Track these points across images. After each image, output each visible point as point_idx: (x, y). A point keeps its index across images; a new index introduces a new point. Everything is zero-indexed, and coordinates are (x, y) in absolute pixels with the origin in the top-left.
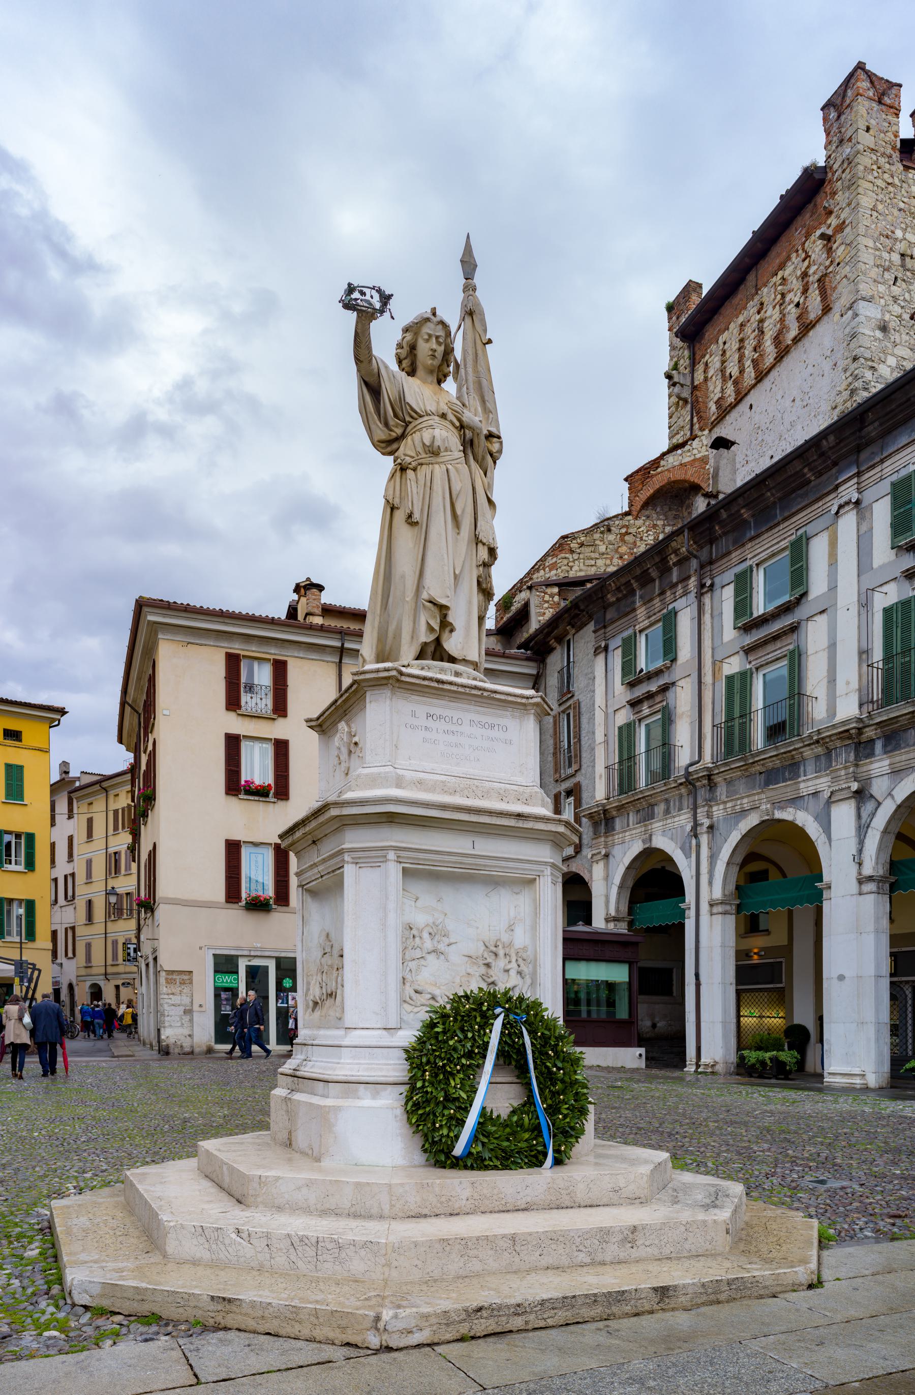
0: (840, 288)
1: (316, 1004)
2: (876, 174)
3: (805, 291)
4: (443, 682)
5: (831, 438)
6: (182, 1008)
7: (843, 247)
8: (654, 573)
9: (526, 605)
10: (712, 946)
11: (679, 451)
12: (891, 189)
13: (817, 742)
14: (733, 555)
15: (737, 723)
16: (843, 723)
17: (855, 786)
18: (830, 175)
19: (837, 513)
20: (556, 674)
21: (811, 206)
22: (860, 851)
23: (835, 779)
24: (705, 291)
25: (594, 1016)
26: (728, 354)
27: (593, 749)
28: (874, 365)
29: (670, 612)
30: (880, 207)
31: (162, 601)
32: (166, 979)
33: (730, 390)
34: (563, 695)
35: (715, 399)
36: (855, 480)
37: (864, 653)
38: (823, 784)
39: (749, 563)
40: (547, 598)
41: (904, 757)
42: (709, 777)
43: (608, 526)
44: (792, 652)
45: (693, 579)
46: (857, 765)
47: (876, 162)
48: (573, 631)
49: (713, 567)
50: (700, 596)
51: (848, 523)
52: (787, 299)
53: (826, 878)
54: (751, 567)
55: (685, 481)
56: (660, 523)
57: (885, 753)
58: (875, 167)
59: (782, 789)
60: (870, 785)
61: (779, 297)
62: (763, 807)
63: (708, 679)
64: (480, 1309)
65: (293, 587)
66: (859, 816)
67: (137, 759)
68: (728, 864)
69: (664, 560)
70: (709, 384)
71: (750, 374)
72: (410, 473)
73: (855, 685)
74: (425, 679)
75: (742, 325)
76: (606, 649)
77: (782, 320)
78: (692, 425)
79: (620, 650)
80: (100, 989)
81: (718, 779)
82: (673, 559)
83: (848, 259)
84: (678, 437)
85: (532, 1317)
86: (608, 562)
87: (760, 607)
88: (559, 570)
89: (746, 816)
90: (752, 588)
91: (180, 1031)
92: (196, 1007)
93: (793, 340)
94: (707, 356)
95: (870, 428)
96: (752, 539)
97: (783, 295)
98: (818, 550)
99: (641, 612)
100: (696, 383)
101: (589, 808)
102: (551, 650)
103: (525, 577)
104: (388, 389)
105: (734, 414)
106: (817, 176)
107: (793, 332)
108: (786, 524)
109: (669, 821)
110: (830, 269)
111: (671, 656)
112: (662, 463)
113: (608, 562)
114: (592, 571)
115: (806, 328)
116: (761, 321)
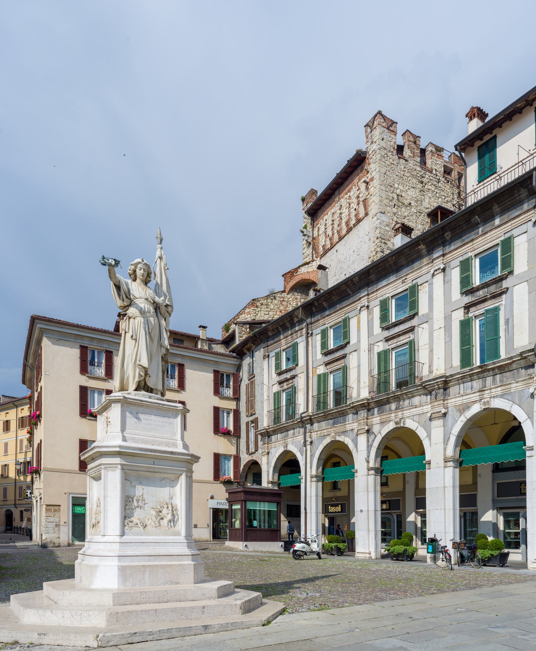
0: (372, 205)
1: (94, 526)
2: (386, 159)
3: (358, 204)
4: (143, 401)
5: (357, 278)
6: (54, 524)
7: (373, 188)
8: (288, 325)
9: (234, 331)
10: (311, 495)
11: (307, 266)
12: (392, 166)
13: (352, 407)
14: (320, 321)
15: (322, 395)
16: (362, 400)
17: (366, 428)
18: (368, 155)
19: (360, 310)
20: (247, 365)
21: (360, 167)
22: (368, 456)
23: (359, 424)
24: (319, 194)
25: (262, 527)
26: (328, 225)
27: (263, 402)
28: (386, 242)
29: (295, 343)
30: (388, 173)
31: (45, 317)
32: (46, 509)
33: (328, 242)
34: (250, 376)
35: (322, 245)
36: (367, 297)
37: (370, 371)
38: (355, 426)
39: (326, 326)
40: (244, 329)
41: (385, 417)
42: (311, 419)
43: (274, 297)
44: (344, 367)
45: (304, 330)
46: (367, 419)
47: (386, 154)
48: (254, 347)
49: (312, 325)
50: (307, 338)
51: (364, 313)
52: (351, 206)
53: (356, 468)
54: (327, 328)
55: (309, 280)
56: (299, 297)
57: (378, 414)
58: (386, 156)
59: (339, 428)
60: (372, 427)
61: (348, 204)
62: (332, 435)
63: (310, 375)
64: (136, 633)
65: (117, 314)
66: (368, 441)
67: (33, 393)
68: (318, 459)
69: (292, 320)
70: (320, 237)
71: (336, 238)
72: (132, 320)
73: (367, 384)
74: (135, 400)
75: (333, 213)
76: (268, 356)
77: (349, 215)
78: (313, 255)
79: (274, 358)
80: (12, 512)
81: (314, 420)
82: (296, 320)
83: (374, 194)
84: (307, 259)
85: (156, 636)
86: (275, 313)
87: (331, 345)
88: (252, 315)
89: (325, 438)
90: (328, 337)
91: (53, 535)
92: (62, 523)
93: (354, 225)
94: (319, 225)
95: (372, 276)
96: (327, 316)
97: (350, 204)
98: (353, 323)
99: (283, 342)
100: (314, 236)
101: (261, 430)
102: (245, 354)
103: (235, 316)
104: (124, 287)
105: (330, 253)
106: (363, 155)
107: (353, 222)
108: (341, 311)
109: (295, 438)
110: (368, 197)
111: (296, 363)
112: (299, 270)
113: (275, 313)
114: (266, 318)
115: (359, 221)
116: (341, 214)
